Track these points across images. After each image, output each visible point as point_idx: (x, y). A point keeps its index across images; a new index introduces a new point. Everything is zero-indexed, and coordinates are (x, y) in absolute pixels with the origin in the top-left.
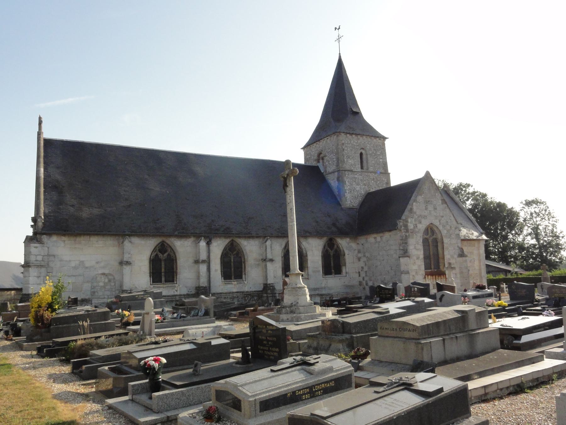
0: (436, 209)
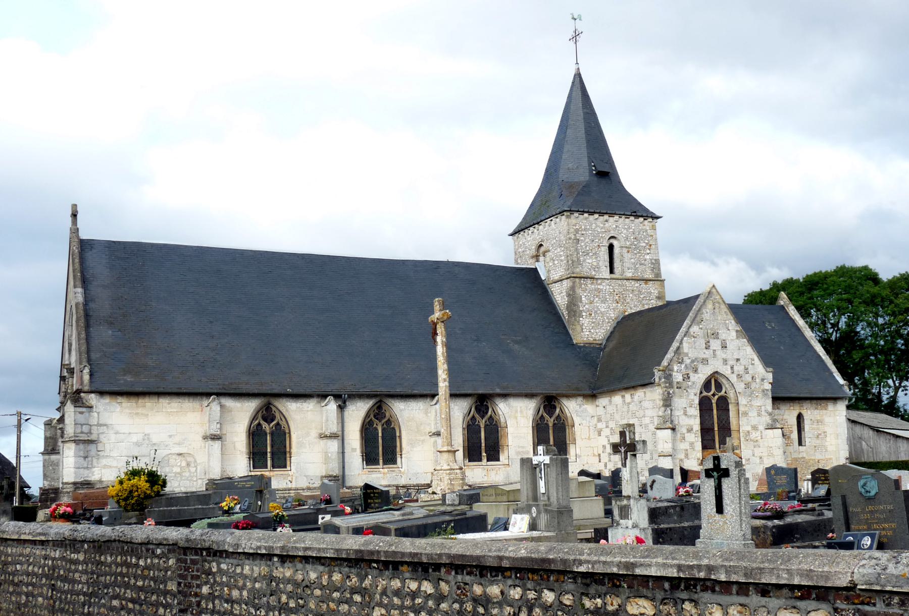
0: (726, 347)
